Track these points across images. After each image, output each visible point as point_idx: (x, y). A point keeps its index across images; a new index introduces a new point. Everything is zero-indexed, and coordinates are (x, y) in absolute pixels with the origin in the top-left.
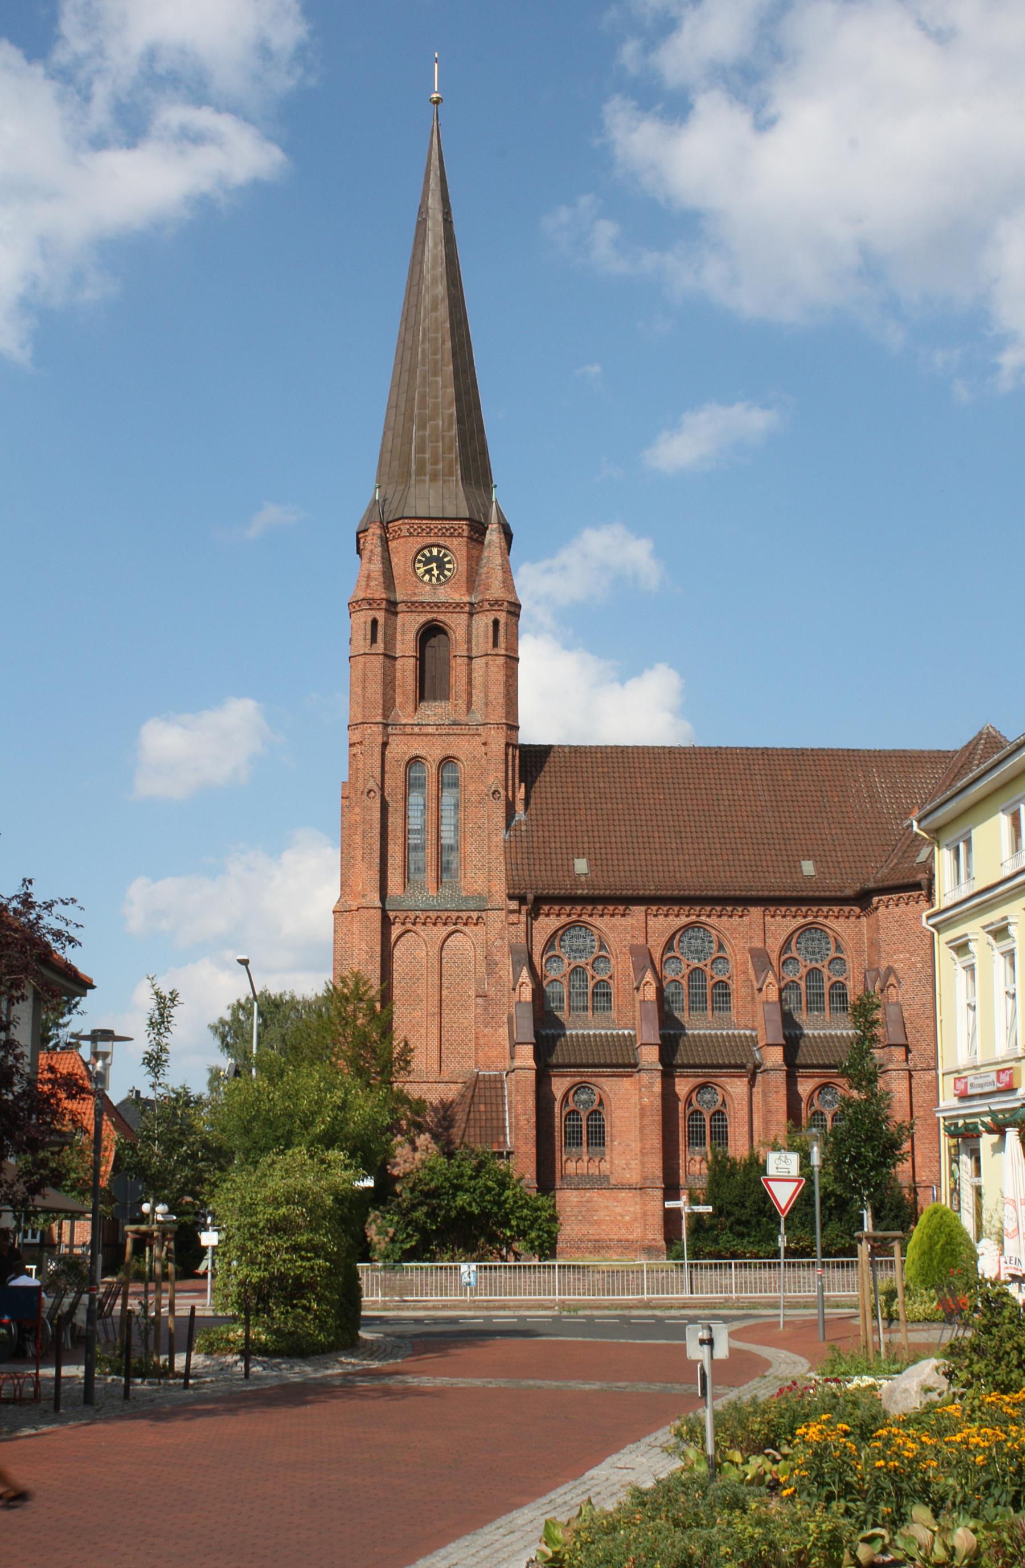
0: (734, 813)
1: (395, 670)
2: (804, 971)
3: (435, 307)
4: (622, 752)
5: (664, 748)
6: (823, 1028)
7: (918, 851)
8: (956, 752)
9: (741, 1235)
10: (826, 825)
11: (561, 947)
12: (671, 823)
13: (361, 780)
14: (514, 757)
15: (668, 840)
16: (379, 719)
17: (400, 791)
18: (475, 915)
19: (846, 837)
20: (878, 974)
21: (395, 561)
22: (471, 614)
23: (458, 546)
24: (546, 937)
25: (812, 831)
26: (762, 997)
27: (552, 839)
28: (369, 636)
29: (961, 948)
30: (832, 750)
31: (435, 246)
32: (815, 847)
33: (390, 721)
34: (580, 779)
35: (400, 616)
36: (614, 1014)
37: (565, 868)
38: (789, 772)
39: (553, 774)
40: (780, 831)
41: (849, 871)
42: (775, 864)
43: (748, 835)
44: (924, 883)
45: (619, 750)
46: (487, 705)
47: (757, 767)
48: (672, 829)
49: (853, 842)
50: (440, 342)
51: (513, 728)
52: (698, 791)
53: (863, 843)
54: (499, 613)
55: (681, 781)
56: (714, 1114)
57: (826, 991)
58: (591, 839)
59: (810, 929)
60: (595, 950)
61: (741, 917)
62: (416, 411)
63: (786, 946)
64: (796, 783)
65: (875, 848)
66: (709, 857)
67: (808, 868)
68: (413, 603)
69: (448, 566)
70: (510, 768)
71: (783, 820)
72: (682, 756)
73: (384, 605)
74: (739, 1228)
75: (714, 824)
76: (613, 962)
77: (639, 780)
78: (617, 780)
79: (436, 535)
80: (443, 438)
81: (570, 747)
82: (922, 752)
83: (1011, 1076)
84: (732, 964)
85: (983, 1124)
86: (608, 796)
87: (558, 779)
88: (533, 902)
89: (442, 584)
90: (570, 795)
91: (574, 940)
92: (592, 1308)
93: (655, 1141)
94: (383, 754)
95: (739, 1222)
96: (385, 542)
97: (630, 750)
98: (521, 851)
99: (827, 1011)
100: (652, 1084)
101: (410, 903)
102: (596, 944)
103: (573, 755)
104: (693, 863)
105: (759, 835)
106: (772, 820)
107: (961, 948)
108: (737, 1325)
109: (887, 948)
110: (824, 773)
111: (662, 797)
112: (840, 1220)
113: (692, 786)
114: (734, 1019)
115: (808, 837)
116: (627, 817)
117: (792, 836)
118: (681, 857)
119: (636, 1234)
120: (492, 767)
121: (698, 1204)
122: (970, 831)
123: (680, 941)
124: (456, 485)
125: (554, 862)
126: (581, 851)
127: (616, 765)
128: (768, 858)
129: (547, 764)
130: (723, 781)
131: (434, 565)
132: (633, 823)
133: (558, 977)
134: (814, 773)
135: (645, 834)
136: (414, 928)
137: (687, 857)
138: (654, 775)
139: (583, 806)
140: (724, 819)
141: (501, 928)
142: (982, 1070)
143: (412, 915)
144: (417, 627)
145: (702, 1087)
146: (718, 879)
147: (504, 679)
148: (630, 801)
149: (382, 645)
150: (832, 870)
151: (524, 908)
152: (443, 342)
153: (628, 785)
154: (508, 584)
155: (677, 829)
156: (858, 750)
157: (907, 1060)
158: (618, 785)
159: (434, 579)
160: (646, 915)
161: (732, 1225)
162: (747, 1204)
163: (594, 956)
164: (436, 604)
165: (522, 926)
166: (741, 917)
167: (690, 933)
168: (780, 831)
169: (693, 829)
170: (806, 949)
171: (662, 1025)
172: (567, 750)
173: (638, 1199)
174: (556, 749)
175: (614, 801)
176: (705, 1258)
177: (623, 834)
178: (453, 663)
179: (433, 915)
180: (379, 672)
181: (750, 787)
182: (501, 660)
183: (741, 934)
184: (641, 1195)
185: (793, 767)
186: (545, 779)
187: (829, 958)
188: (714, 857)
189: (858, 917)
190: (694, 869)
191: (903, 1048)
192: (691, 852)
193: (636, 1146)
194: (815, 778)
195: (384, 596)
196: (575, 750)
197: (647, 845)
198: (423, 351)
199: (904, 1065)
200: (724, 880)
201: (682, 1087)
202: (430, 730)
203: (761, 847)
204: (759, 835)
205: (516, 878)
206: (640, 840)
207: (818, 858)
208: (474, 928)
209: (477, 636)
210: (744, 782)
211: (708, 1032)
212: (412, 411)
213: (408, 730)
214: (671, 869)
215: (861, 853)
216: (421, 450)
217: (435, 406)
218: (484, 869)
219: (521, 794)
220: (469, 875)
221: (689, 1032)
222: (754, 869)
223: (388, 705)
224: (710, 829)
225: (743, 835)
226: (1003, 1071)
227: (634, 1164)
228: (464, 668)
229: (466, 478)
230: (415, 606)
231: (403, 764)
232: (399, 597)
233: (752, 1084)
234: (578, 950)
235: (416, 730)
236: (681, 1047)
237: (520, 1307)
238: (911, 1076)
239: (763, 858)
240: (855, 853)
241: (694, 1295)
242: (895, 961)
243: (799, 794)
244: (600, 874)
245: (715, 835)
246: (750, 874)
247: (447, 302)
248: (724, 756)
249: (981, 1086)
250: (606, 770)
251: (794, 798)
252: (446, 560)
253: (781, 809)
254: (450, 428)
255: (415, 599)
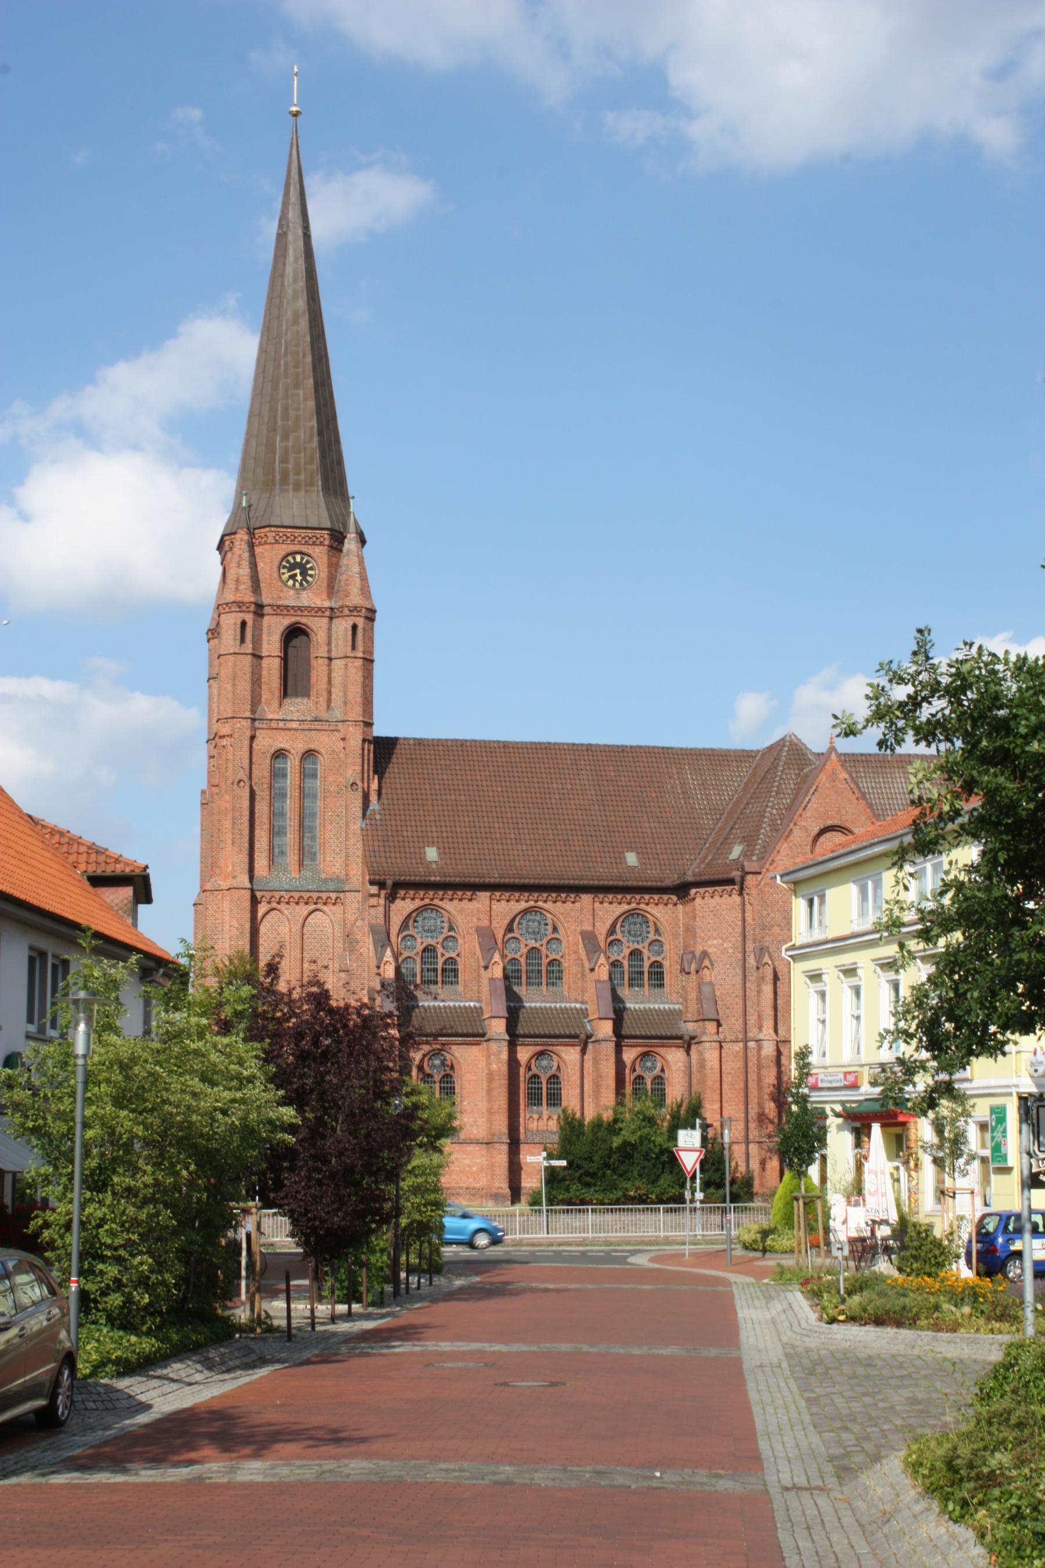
0: (564, 806)
1: (261, 668)
2: (627, 952)
3: (296, 321)
4: (462, 745)
5: (499, 742)
6: (642, 1002)
7: (730, 850)
8: (758, 751)
9: (588, 1185)
10: (646, 819)
11: (415, 927)
12: (509, 815)
13: (230, 770)
14: (369, 751)
15: (507, 831)
16: (248, 714)
17: (266, 781)
18: (333, 896)
19: (663, 830)
20: (694, 956)
21: (261, 565)
22: (331, 618)
23: (320, 554)
24: (402, 919)
25: (633, 824)
26: (594, 975)
27: (404, 828)
28: (239, 637)
29: (815, 977)
30: (649, 747)
31: (296, 259)
32: (637, 840)
33: (257, 716)
34: (425, 771)
35: (266, 618)
36: (460, 988)
37: (418, 856)
38: (611, 768)
39: (400, 766)
40: (605, 824)
41: (667, 862)
42: (603, 855)
43: (577, 827)
44: (738, 879)
45: (459, 744)
46: (345, 703)
47: (582, 762)
48: (510, 820)
49: (669, 835)
50: (301, 355)
51: (369, 725)
52: (532, 785)
53: (679, 836)
54: (358, 619)
55: (516, 774)
56: (550, 1078)
57: (646, 969)
58: (439, 829)
59: (632, 915)
60: (445, 930)
61: (573, 902)
62: (279, 423)
63: (612, 931)
64: (618, 778)
65: (690, 841)
66: (544, 847)
67: (632, 859)
68: (278, 607)
69: (310, 572)
70: (366, 762)
71: (608, 813)
72: (516, 750)
73: (252, 608)
74: (588, 1179)
75: (547, 816)
76: (460, 941)
77: (478, 773)
78: (459, 772)
79: (300, 543)
80: (305, 449)
81: (415, 739)
82: (729, 751)
83: (856, 1077)
84: (564, 944)
85: (833, 1110)
86: (452, 787)
87: (406, 771)
88: (392, 888)
89: (304, 589)
90: (418, 786)
91: (429, 920)
92: (533, 1245)
93: (501, 1101)
94: (251, 747)
95: (588, 1174)
96: (251, 546)
97: (468, 744)
98: (379, 838)
99: (646, 987)
100: (500, 1052)
101: (274, 884)
102: (446, 925)
103: (417, 747)
104: (530, 853)
105: (587, 828)
106: (598, 813)
107: (815, 977)
108: (652, 1255)
109: (703, 934)
110: (643, 769)
111: (499, 789)
112: (671, 1172)
113: (526, 780)
114: (566, 993)
115: (630, 829)
116: (469, 808)
117: (616, 829)
118: (519, 847)
119: (482, 1182)
120: (350, 760)
121: (552, 1159)
122: (824, 890)
123: (519, 923)
124: (317, 496)
125: (407, 850)
126: (430, 840)
127: (456, 758)
128: (596, 849)
129: (394, 756)
130: (553, 776)
131: (298, 571)
132: (475, 814)
133: (412, 954)
134: (634, 769)
135: (486, 825)
136: (278, 907)
137: (524, 847)
138: (491, 769)
139: (429, 797)
140: (556, 811)
141: (359, 909)
142: (830, 1070)
143: (277, 895)
144: (282, 629)
145: (540, 1054)
146: (553, 869)
147: (361, 680)
148: (471, 793)
149: (251, 646)
150: (652, 861)
151: (383, 893)
152: (304, 356)
153: (469, 777)
154: (365, 591)
155: (515, 820)
156: (672, 748)
157: (718, 1033)
158: (460, 777)
159: (297, 585)
160: (491, 899)
161: (581, 1175)
162: (595, 1159)
163: (443, 936)
164: (300, 608)
165: (381, 909)
166: (573, 902)
167: (529, 916)
168: (605, 824)
169: (529, 821)
170: (629, 932)
171: (508, 999)
172: (412, 742)
173: (484, 1152)
174: (401, 742)
175: (457, 792)
176: (558, 1204)
177: (467, 824)
178: (314, 663)
179: (296, 895)
180: (248, 670)
181: (577, 782)
182: (359, 663)
183: (576, 918)
184: (488, 1149)
185: (615, 763)
186: (393, 770)
187: (649, 940)
188: (548, 848)
189: (675, 904)
190: (531, 858)
191: (715, 1023)
192: (528, 842)
193: (483, 1106)
194: (635, 774)
195: (252, 600)
196: (420, 742)
197: (488, 835)
198: (286, 364)
199: (716, 1038)
200: (558, 869)
201: (524, 1054)
202: (294, 725)
203: (590, 838)
204: (587, 828)
205: (375, 865)
206: (483, 830)
207: (640, 850)
208: (333, 907)
209: (337, 639)
210: (572, 777)
211: (543, 1005)
212: (276, 422)
213: (274, 725)
214: (512, 858)
215: (677, 846)
216: (285, 460)
217: (297, 419)
218: (342, 848)
219: (375, 785)
220: (328, 859)
221: (527, 1005)
222: (584, 859)
223: (255, 701)
224: (543, 822)
225: (573, 827)
226: (850, 1073)
227: (482, 1121)
228: (325, 668)
229: (326, 488)
230: (280, 609)
231: (269, 756)
232: (266, 600)
233: (583, 1052)
234: (429, 931)
235: (281, 725)
236: (521, 1019)
237: (551, 1245)
238: (721, 1047)
239: (592, 849)
240: (672, 846)
241: (550, 1235)
242: (710, 946)
243: (621, 789)
244: (448, 862)
245: (549, 827)
246: (581, 864)
247: (307, 316)
248: (553, 752)
249: (830, 1082)
250: (448, 762)
251: (617, 793)
252: (308, 566)
253: (606, 803)
254: (311, 440)
255: (280, 603)
